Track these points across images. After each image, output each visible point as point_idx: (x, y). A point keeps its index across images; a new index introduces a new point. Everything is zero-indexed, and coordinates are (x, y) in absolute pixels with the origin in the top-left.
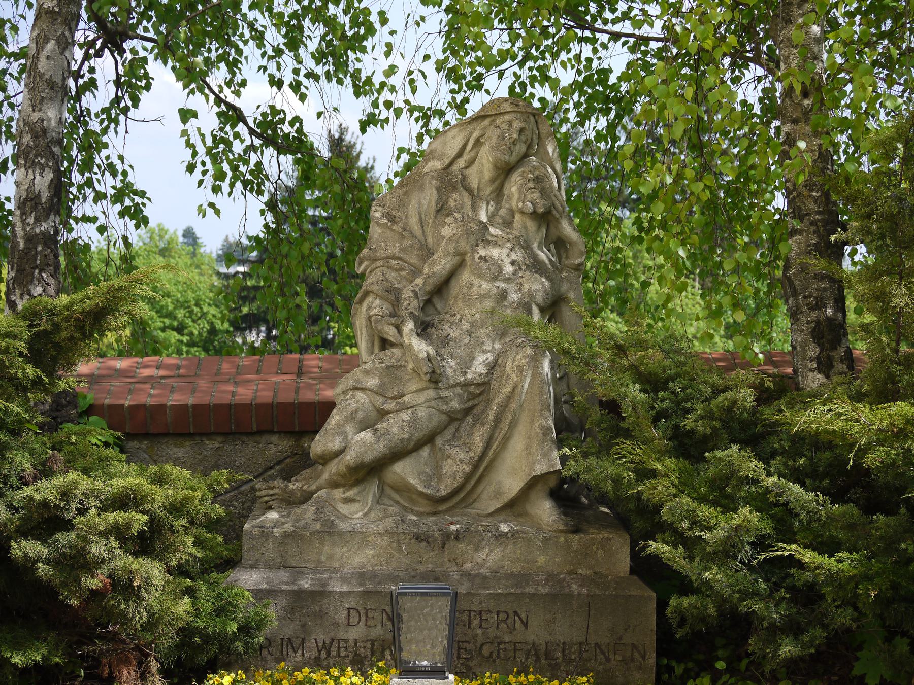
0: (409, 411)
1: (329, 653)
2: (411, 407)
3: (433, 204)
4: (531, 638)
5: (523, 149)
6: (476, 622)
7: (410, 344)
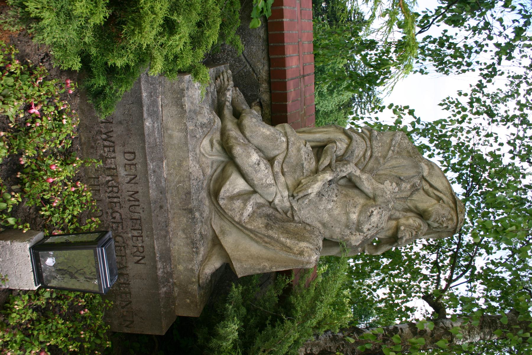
0: (273, 182)
1: (105, 140)
2: (276, 182)
4: (131, 265)
6: (136, 233)
7: (317, 181)
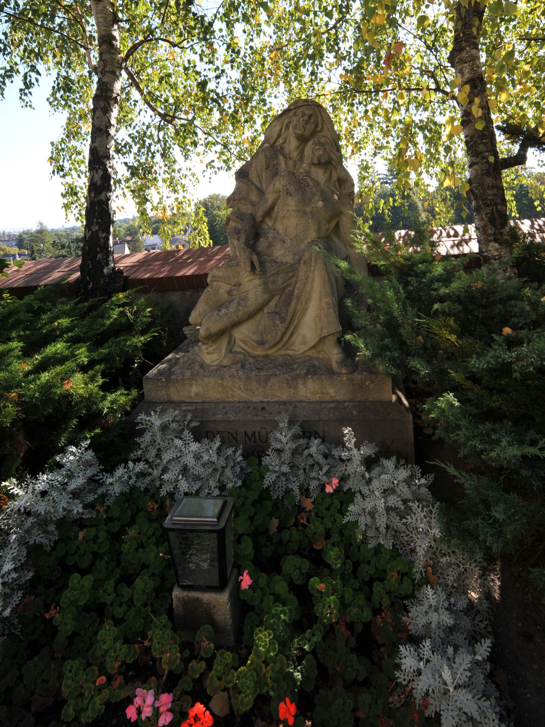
3: (264, 164)
5: (313, 127)
